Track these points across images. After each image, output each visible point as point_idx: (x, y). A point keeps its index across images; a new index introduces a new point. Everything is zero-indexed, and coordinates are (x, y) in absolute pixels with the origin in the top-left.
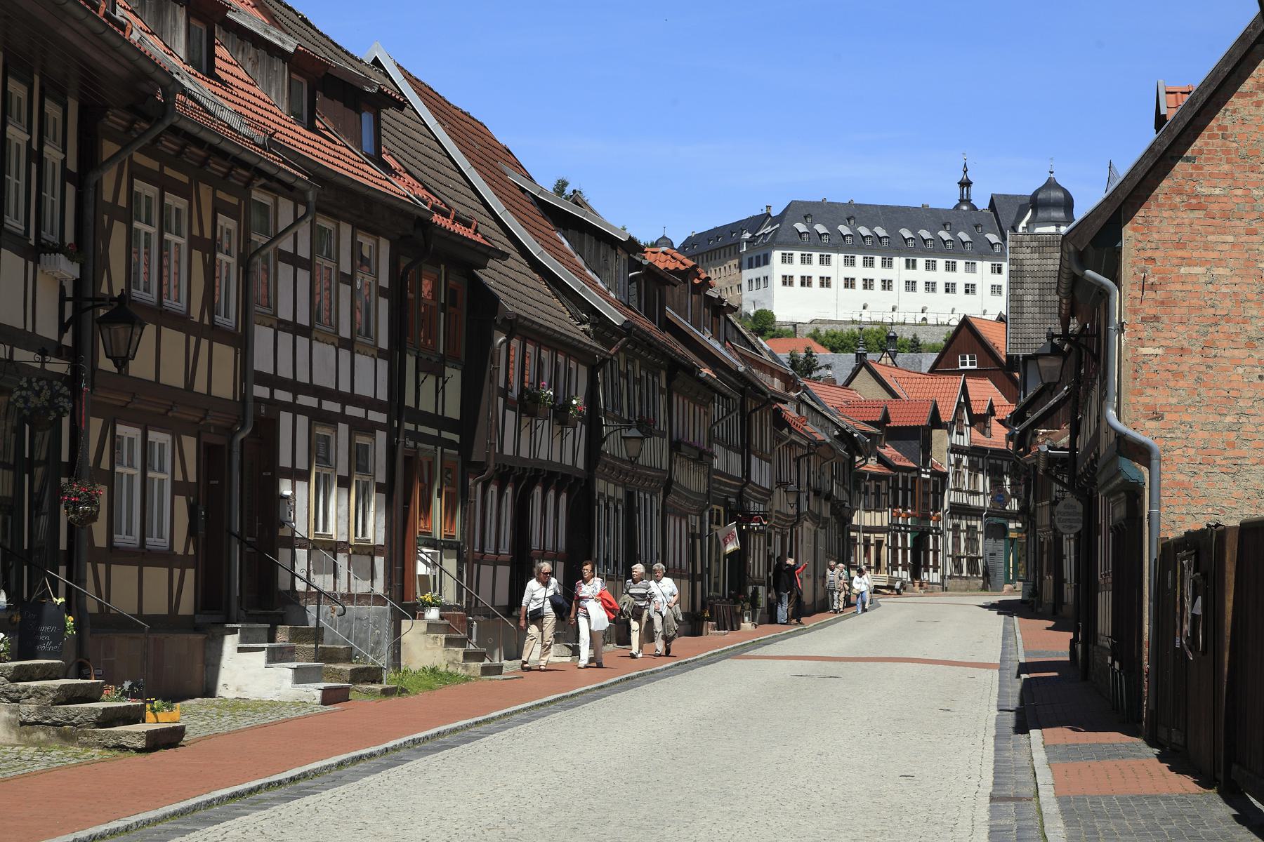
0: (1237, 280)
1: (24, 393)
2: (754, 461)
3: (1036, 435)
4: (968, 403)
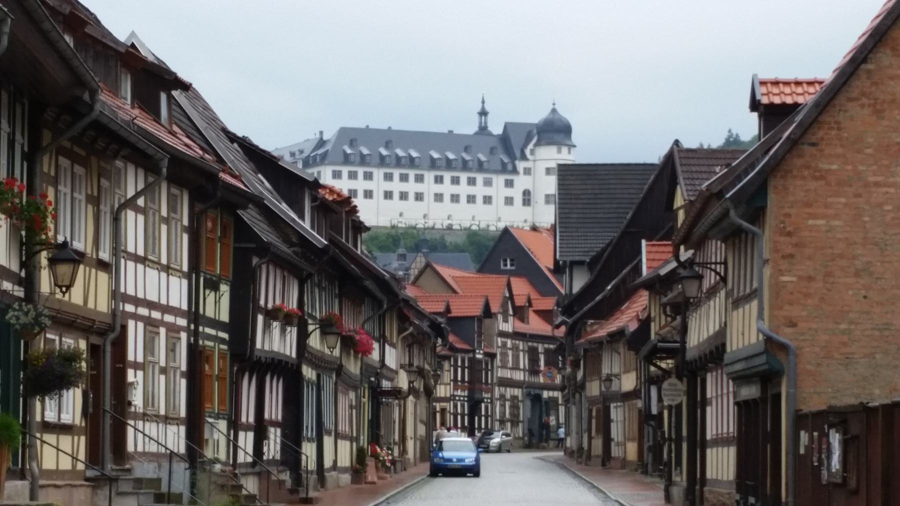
0: (848, 229)
1: (16, 313)
2: (387, 347)
3: (586, 323)
4: (511, 297)
